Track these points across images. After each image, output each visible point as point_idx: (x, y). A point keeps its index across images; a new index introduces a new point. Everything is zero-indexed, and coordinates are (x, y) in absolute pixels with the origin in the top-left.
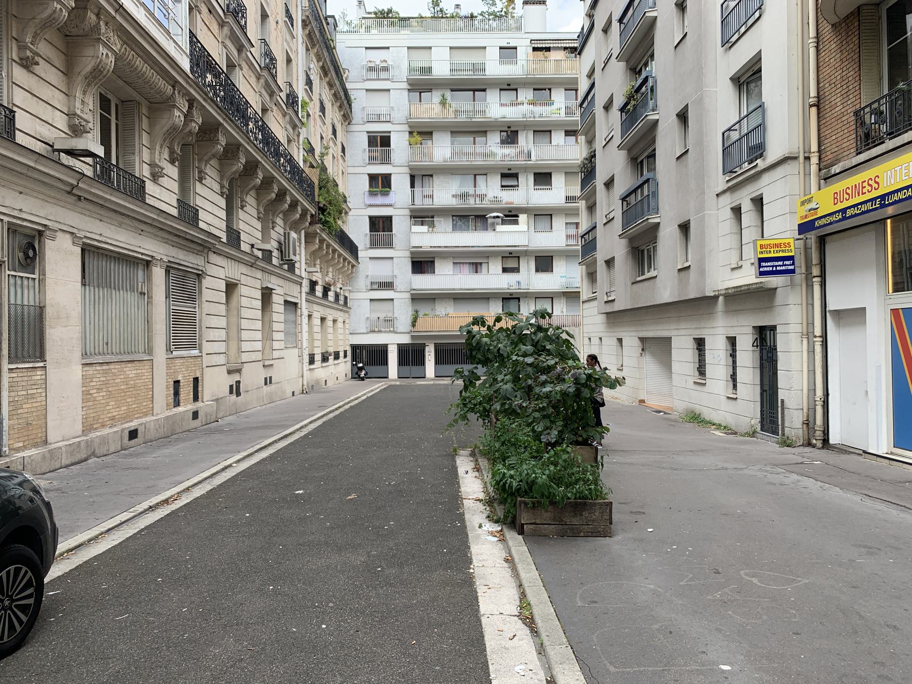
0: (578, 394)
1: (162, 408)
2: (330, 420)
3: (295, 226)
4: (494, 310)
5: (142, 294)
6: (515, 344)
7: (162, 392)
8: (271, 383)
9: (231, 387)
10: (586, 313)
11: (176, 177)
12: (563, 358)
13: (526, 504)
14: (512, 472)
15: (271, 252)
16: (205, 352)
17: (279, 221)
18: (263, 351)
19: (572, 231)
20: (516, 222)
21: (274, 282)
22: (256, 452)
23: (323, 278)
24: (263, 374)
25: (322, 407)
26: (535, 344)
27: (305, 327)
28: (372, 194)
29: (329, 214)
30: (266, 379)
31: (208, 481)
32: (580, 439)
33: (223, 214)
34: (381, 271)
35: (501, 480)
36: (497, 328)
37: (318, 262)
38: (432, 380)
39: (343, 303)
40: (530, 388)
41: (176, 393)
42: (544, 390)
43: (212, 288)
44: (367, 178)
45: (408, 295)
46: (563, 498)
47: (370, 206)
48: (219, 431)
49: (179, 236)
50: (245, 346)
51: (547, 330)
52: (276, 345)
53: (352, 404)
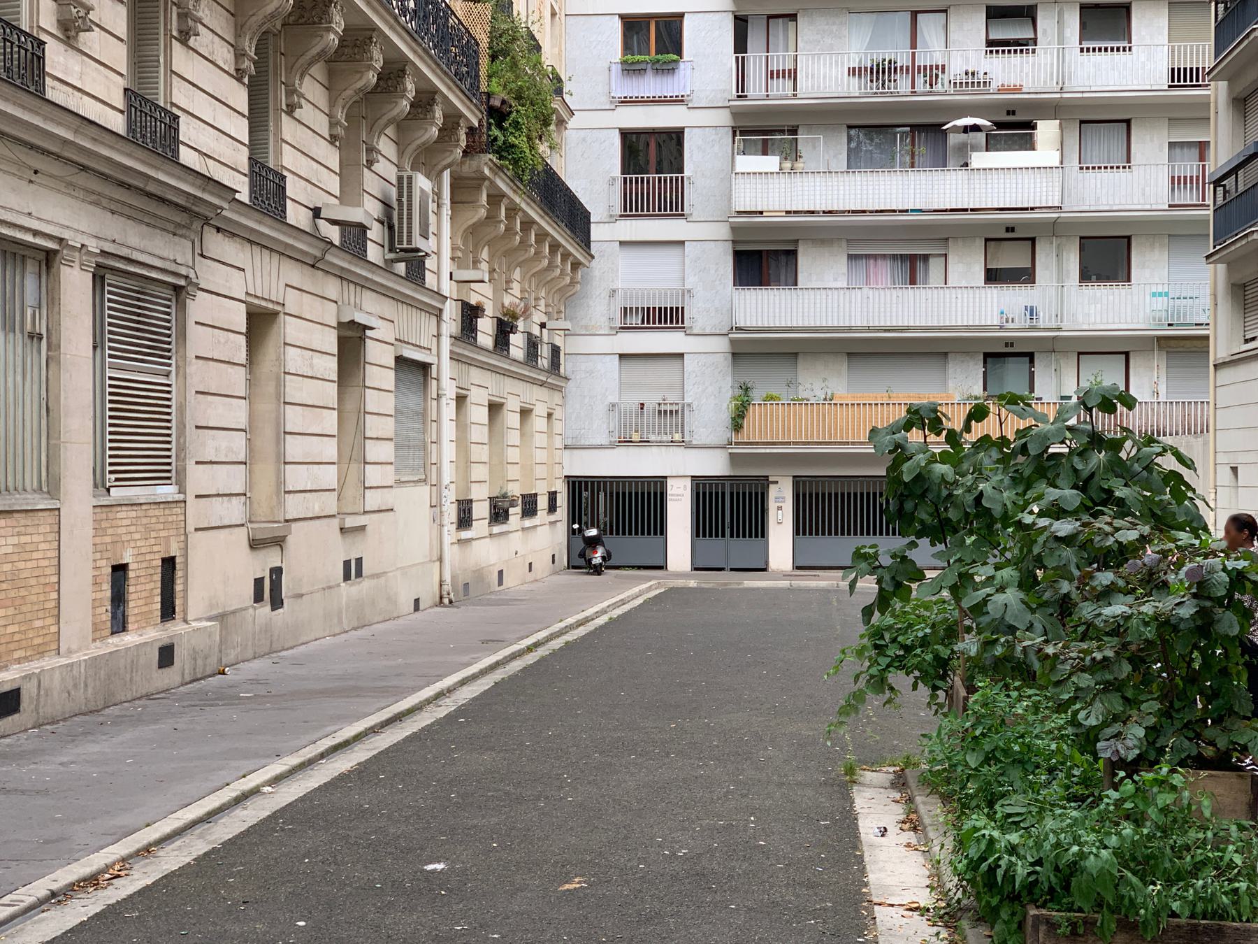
0: (1204, 625)
1: (80, 638)
2: (513, 678)
3: (426, 159)
4: (959, 388)
5: (35, 337)
6: (1023, 482)
7: (83, 593)
8: (359, 574)
9: (259, 582)
10: (1224, 397)
11: (122, 29)
12: (1162, 522)
13: (1052, 926)
14: (1014, 838)
15: (363, 228)
16: (192, 489)
17: (386, 146)
18: (340, 491)
19: (1188, 166)
20: (1028, 144)
21: (370, 310)
22: (322, 756)
23: (496, 299)
24: (341, 551)
25: (491, 643)
26: (1083, 484)
27: (449, 430)
28: (630, 69)
29: (516, 125)
30: (347, 564)
31: (198, 830)
32: (1209, 752)
33: (241, 129)
34: (649, 279)
35: (983, 859)
36: (972, 437)
37: (485, 254)
38: (786, 576)
39: (547, 365)
40: (1065, 606)
41: (119, 598)
42: (1107, 611)
43: (213, 323)
44: (617, 25)
45: (722, 345)
46: (1157, 914)
47: (625, 102)
48: (227, 698)
49: (129, 187)
50: (297, 477)
51: (1116, 445)
52: (374, 475)
53: (569, 637)
